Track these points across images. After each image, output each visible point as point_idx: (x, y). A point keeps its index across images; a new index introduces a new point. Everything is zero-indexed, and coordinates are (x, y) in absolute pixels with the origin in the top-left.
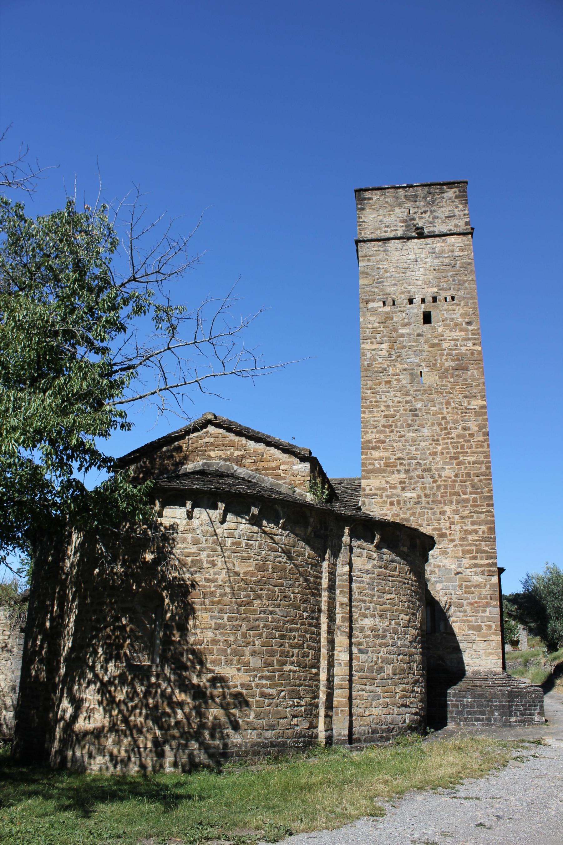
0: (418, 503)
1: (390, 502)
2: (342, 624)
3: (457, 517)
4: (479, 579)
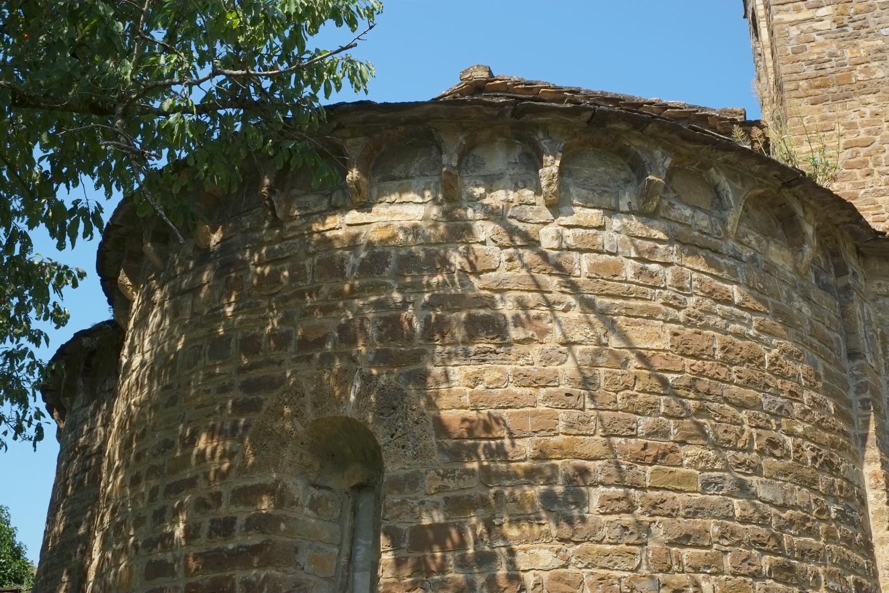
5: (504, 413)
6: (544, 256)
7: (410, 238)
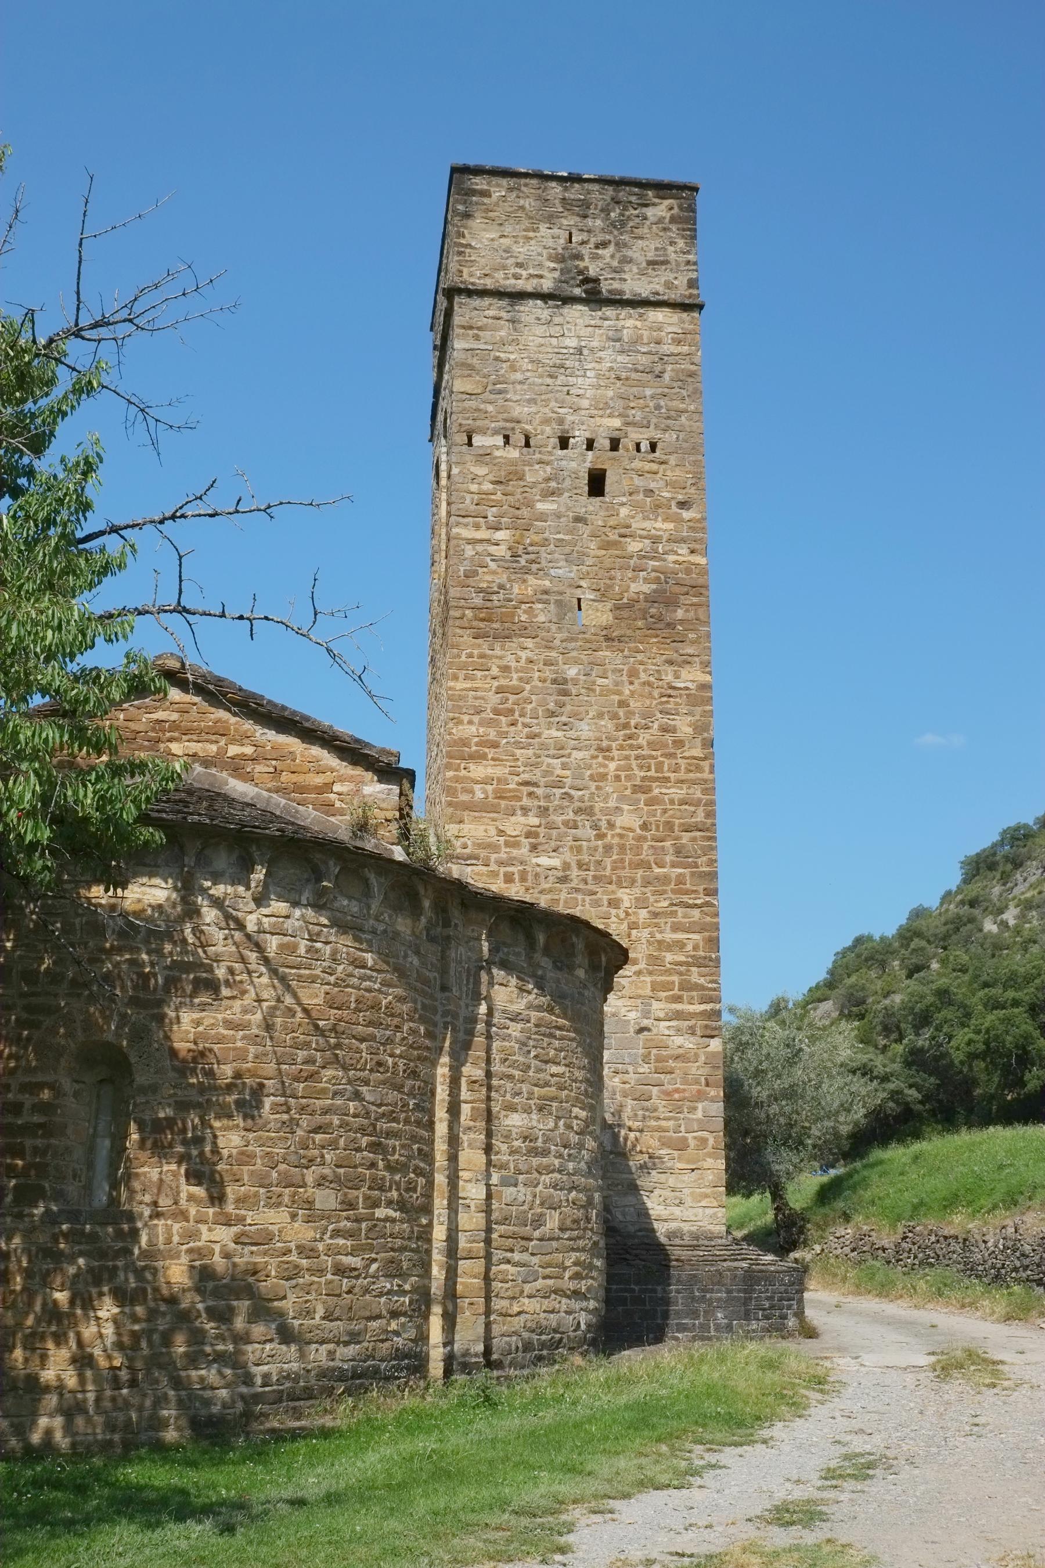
0: (564, 880)
1: (505, 875)
2: (472, 1123)
3: (643, 913)
4: (687, 1043)
5: (215, 1047)
6: (248, 936)
7: (156, 915)
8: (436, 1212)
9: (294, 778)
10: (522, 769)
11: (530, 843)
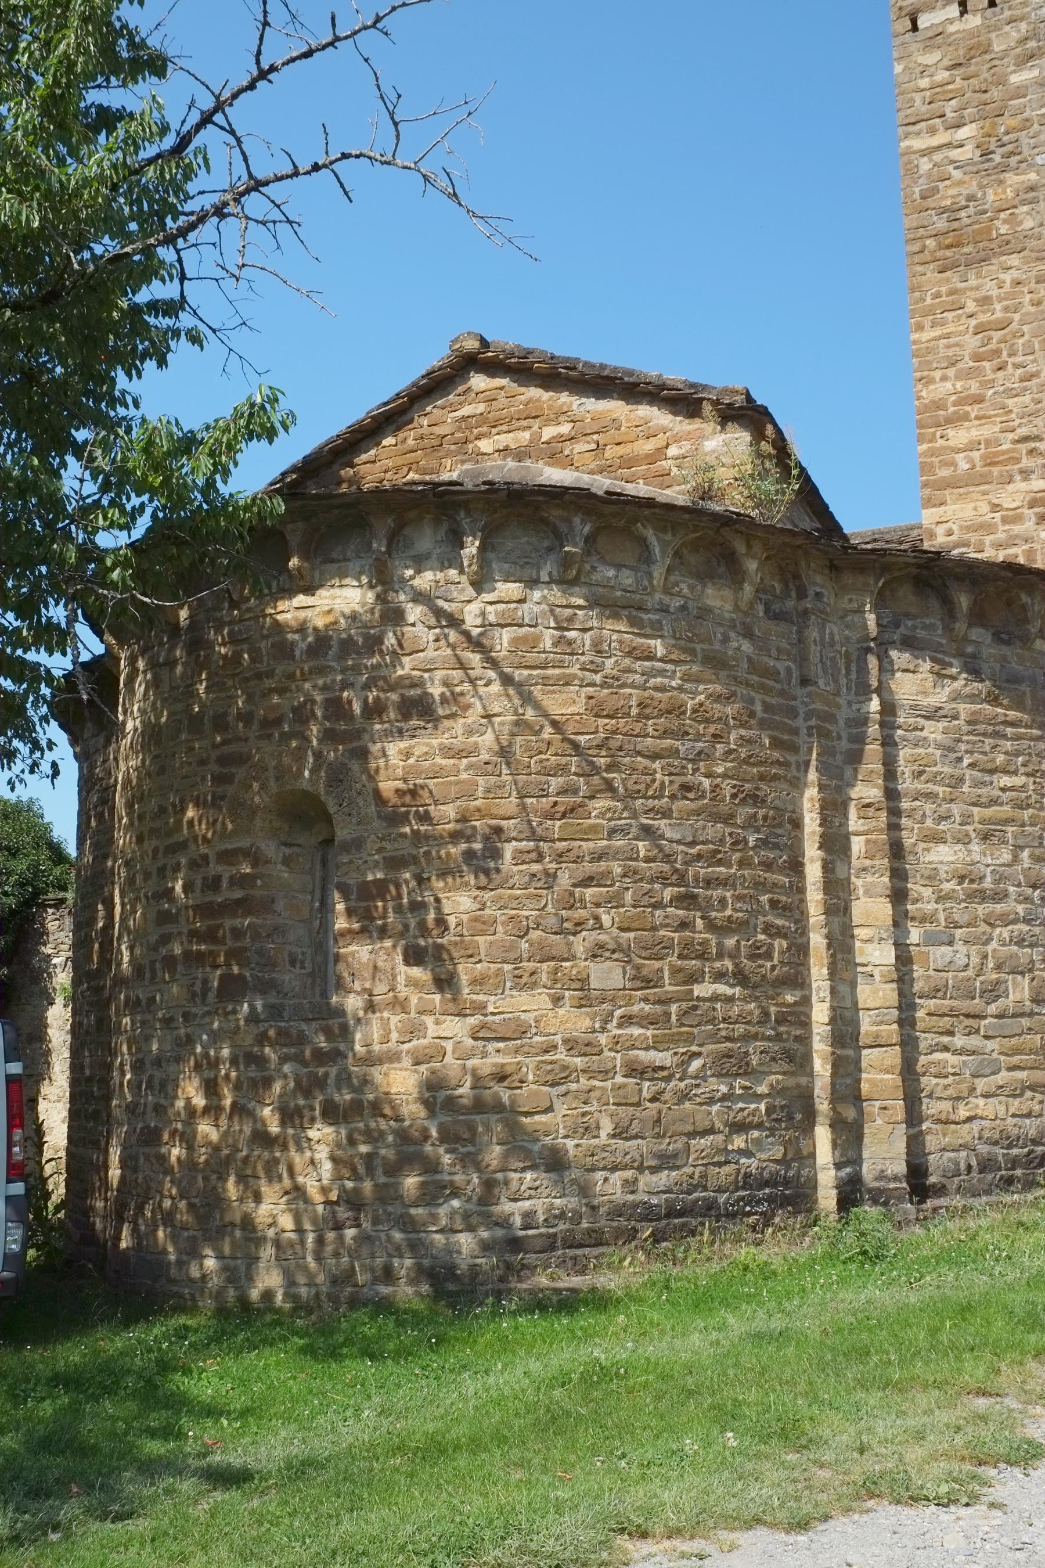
2: (868, 862)
5: (431, 783)
6: (467, 634)
8: (814, 986)
9: (620, 450)
10: (1016, 423)
11: (1036, 514)
